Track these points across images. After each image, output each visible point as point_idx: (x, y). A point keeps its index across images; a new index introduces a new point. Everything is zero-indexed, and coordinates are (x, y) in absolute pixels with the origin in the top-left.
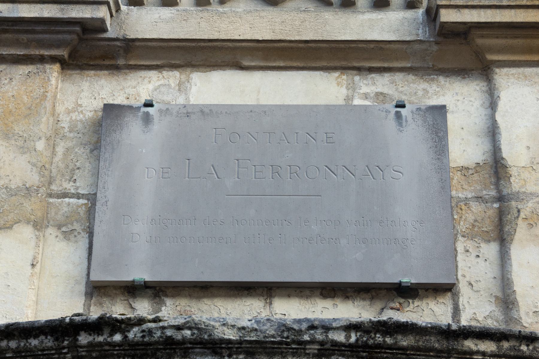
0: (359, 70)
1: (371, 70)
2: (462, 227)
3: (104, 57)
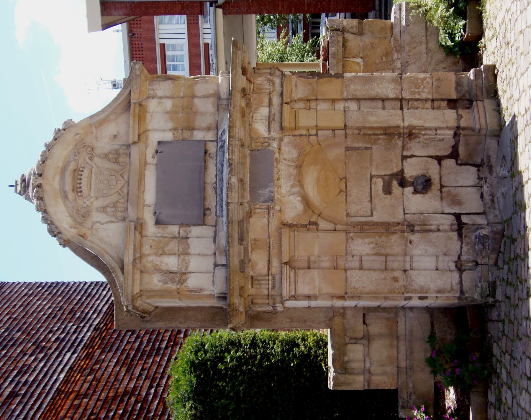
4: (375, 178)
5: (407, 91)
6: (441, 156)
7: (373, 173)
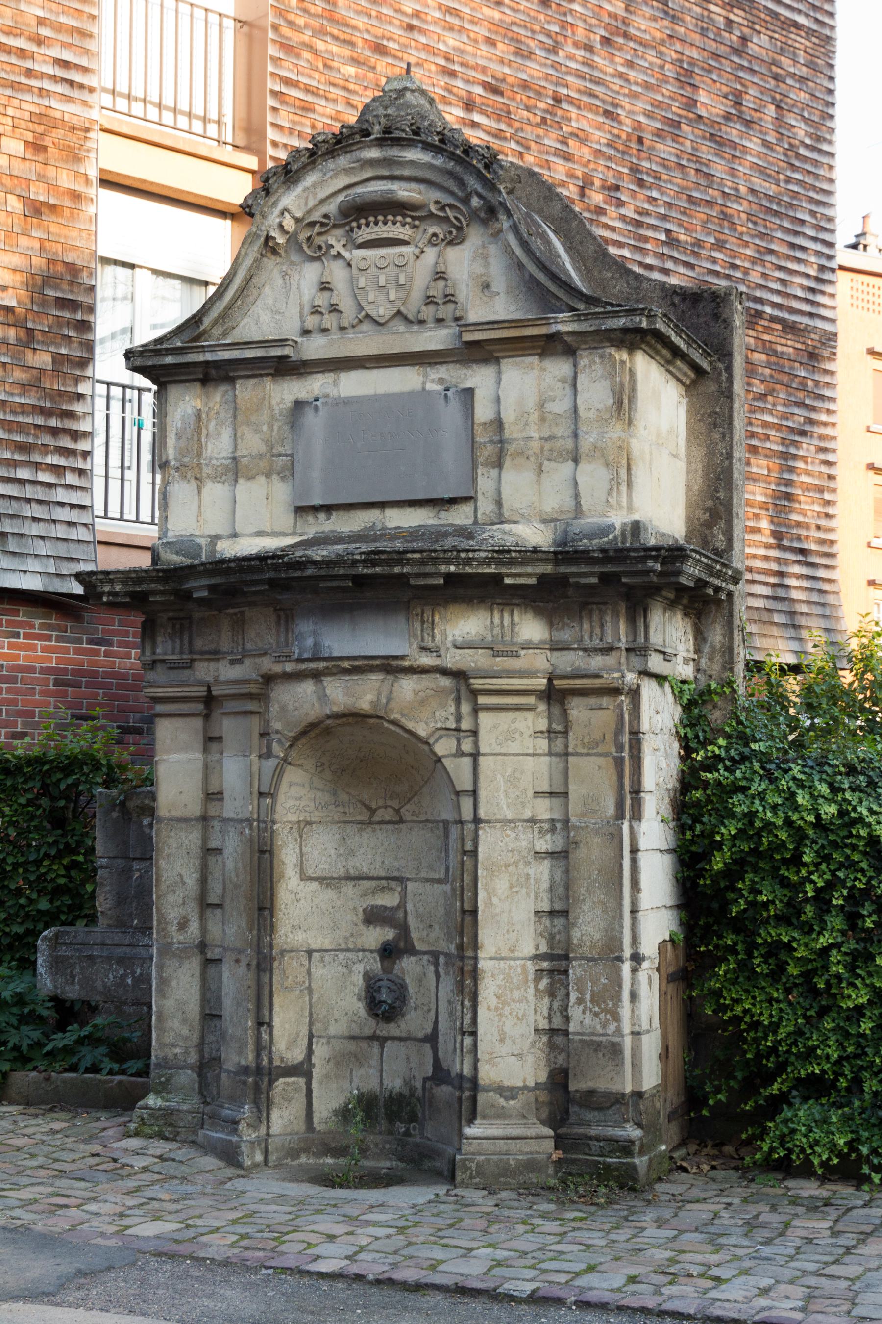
0: (430, 364)
1: (436, 364)
2: (481, 460)
3: (293, 369)
4: (399, 889)
5: (586, 971)
6: (437, 1042)
7: (410, 885)
